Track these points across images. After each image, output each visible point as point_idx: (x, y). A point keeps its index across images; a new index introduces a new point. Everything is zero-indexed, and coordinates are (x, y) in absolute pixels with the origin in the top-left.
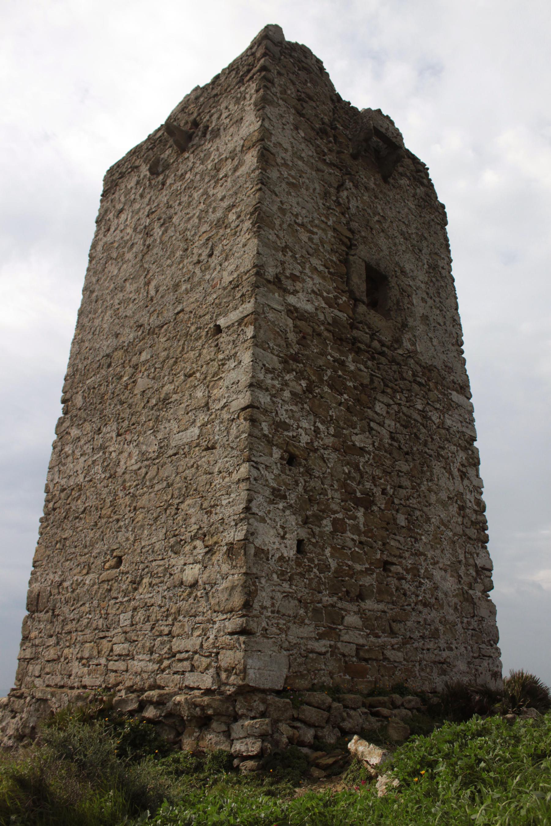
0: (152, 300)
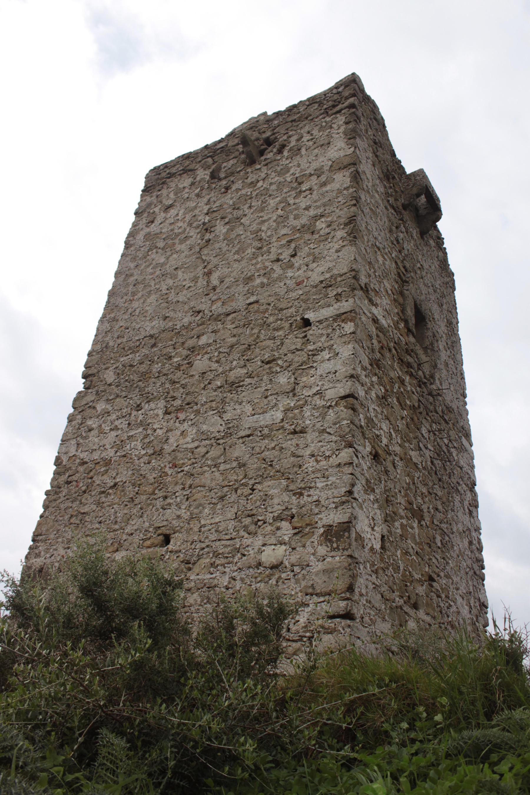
0: (214, 289)
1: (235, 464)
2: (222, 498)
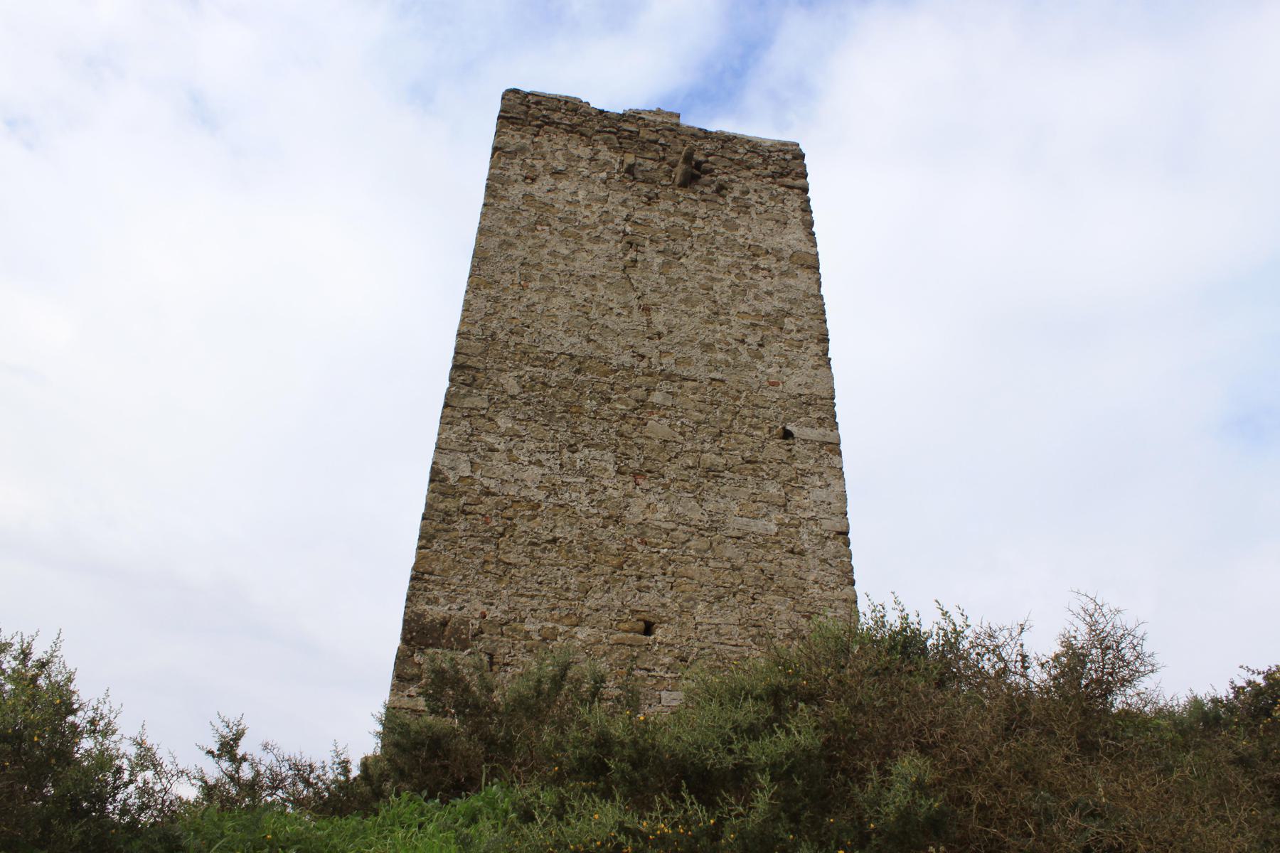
1: (728, 565)
2: (719, 598)
